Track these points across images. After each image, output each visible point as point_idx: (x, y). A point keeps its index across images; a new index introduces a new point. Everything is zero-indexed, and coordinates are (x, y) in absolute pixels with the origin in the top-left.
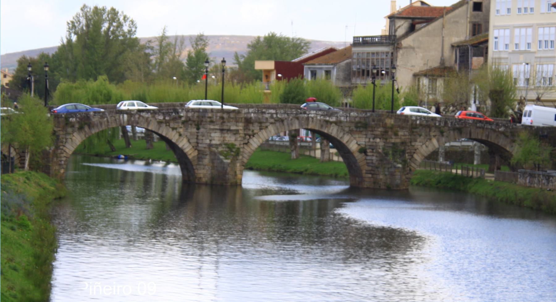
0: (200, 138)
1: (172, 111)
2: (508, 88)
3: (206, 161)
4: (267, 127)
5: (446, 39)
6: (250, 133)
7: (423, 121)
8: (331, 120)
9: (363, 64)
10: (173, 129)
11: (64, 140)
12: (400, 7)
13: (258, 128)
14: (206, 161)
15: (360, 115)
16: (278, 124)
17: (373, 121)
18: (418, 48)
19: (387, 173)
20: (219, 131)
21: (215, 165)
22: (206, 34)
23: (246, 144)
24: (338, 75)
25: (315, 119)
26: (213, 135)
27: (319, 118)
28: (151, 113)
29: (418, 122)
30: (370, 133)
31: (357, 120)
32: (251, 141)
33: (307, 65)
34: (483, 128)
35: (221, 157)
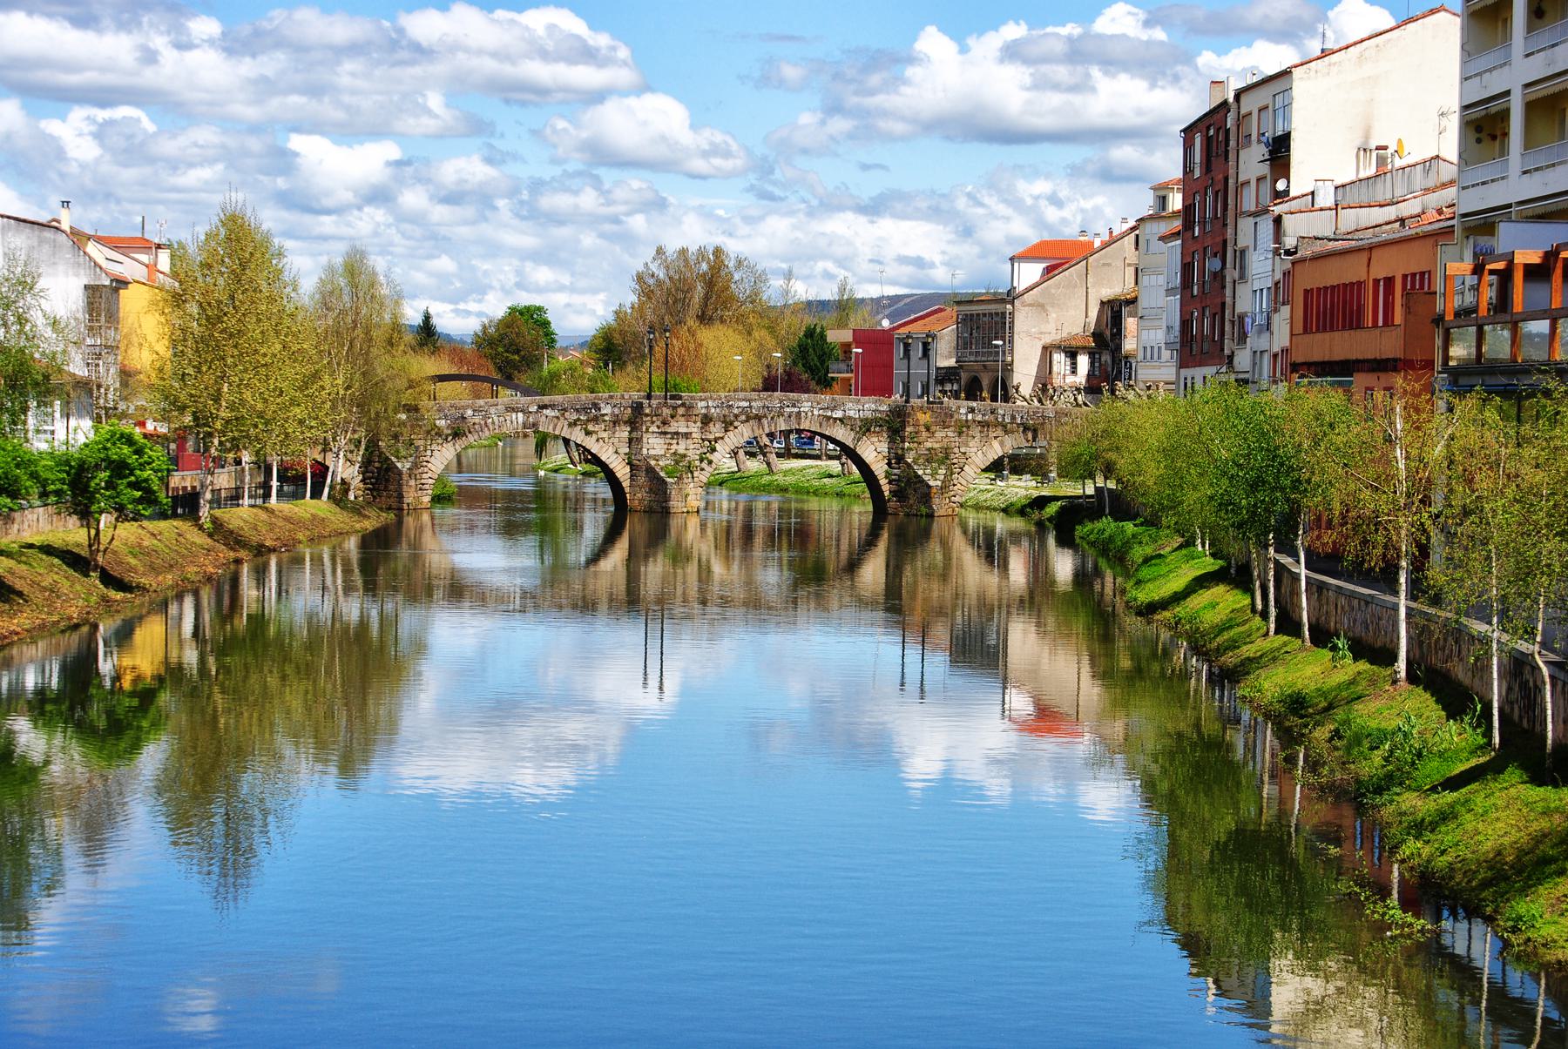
12: (1111, 233)
22: (1453, 103)
27: (816, 412)
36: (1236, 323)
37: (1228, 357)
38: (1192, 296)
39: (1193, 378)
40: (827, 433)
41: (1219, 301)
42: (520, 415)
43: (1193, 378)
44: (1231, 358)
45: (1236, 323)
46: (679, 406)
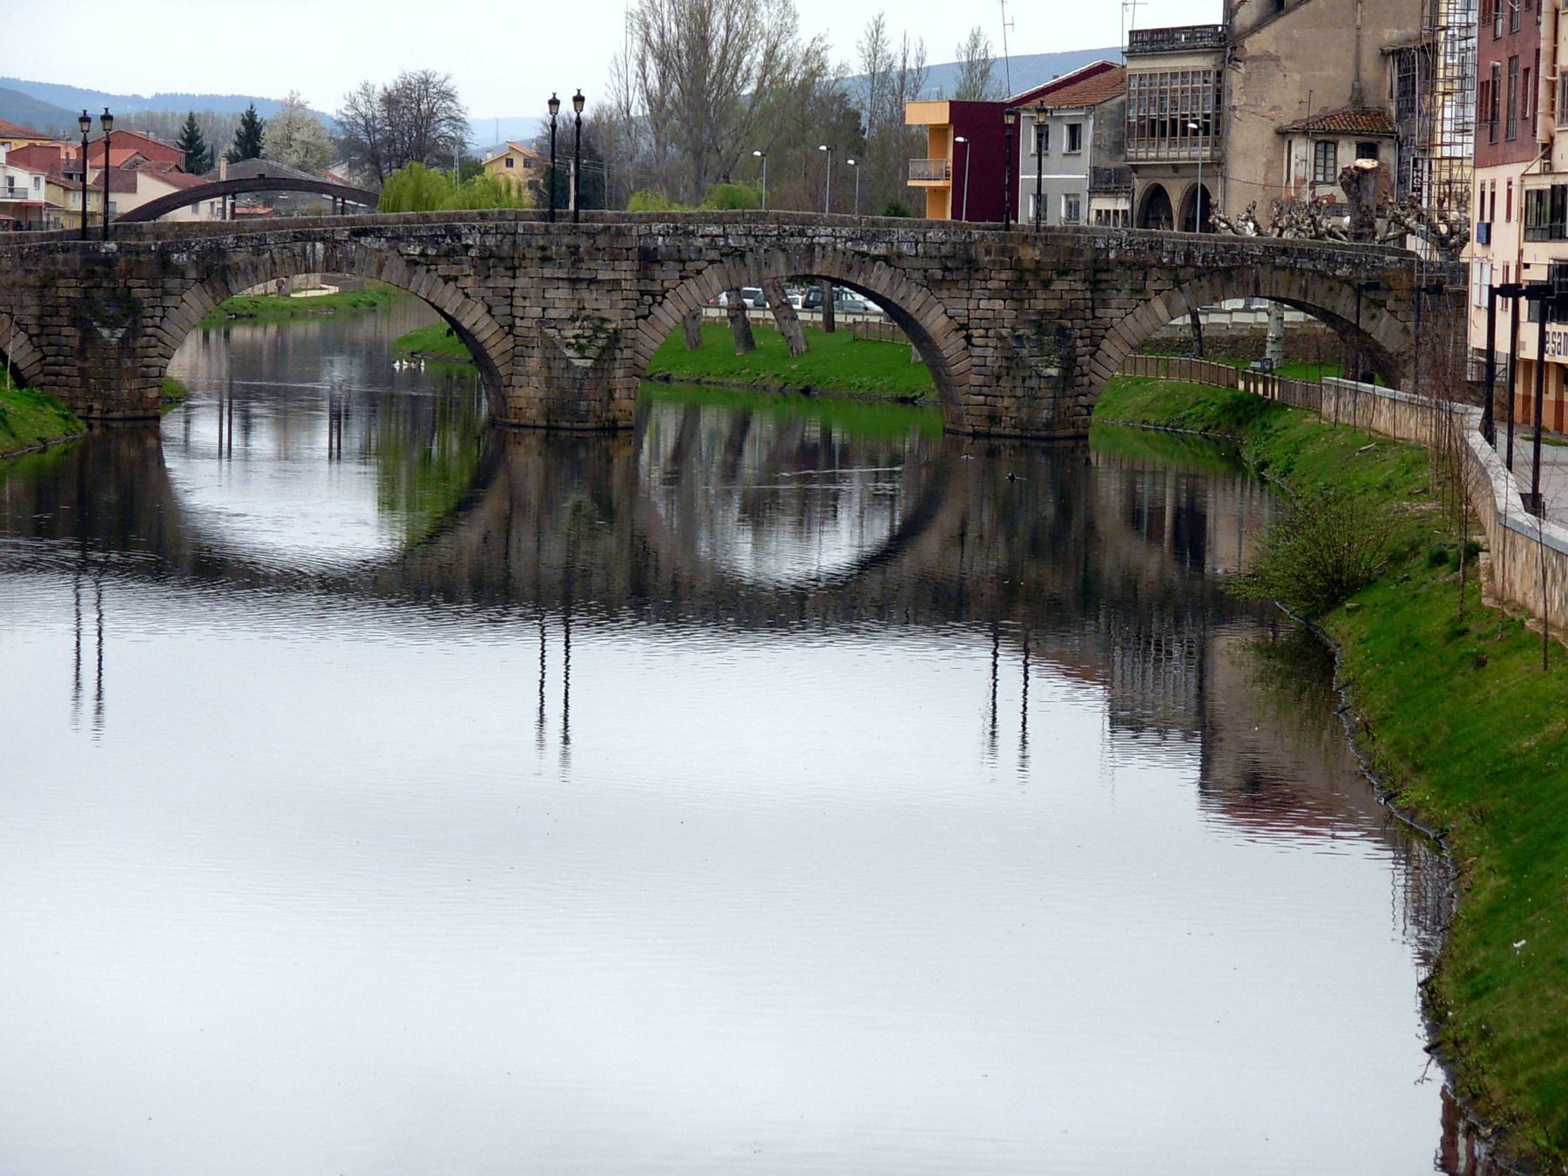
0: (518, 302)
1: (444, 233)
2: (336, 141)
3: (534, 362)
4: (699, 272)
5: (1368, 33)
6: (657, 288)
7: (1126, 251)
8: (874, 252)
9: (1152, 102)
10: (447, 279)
11: (159, 312)
13: (677, 275)
14: (534, 362)
15: (953, 239)
16: (728, 263)
17: (988, 253)
18: (1290, 58)
19: (1019, 392)
20: (566, 284)
21: (555, 373)
23: (645, 317)
24: (1096, 137)
25: (830, 248)
26: (550, 294)
28: (388, 239)
29: (1112, 255)
30: (978, 284)
31: (945, 250)
32: (656, 310)
33: (1025, 109)
34: (1292, 269)
35: (570, 353)
36: (1559, 85)
37: (1544, 146)
38: (1496, 39)
39: (1493, 185)
40: (860, 283)
41: (1532, 46)
42: (319, 246)
43: (1493, 185)
44: (1548, 148)
45: (1559, 85)
46: (599, 233)
